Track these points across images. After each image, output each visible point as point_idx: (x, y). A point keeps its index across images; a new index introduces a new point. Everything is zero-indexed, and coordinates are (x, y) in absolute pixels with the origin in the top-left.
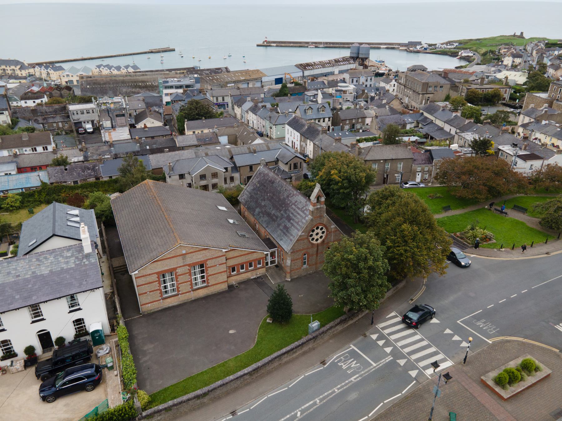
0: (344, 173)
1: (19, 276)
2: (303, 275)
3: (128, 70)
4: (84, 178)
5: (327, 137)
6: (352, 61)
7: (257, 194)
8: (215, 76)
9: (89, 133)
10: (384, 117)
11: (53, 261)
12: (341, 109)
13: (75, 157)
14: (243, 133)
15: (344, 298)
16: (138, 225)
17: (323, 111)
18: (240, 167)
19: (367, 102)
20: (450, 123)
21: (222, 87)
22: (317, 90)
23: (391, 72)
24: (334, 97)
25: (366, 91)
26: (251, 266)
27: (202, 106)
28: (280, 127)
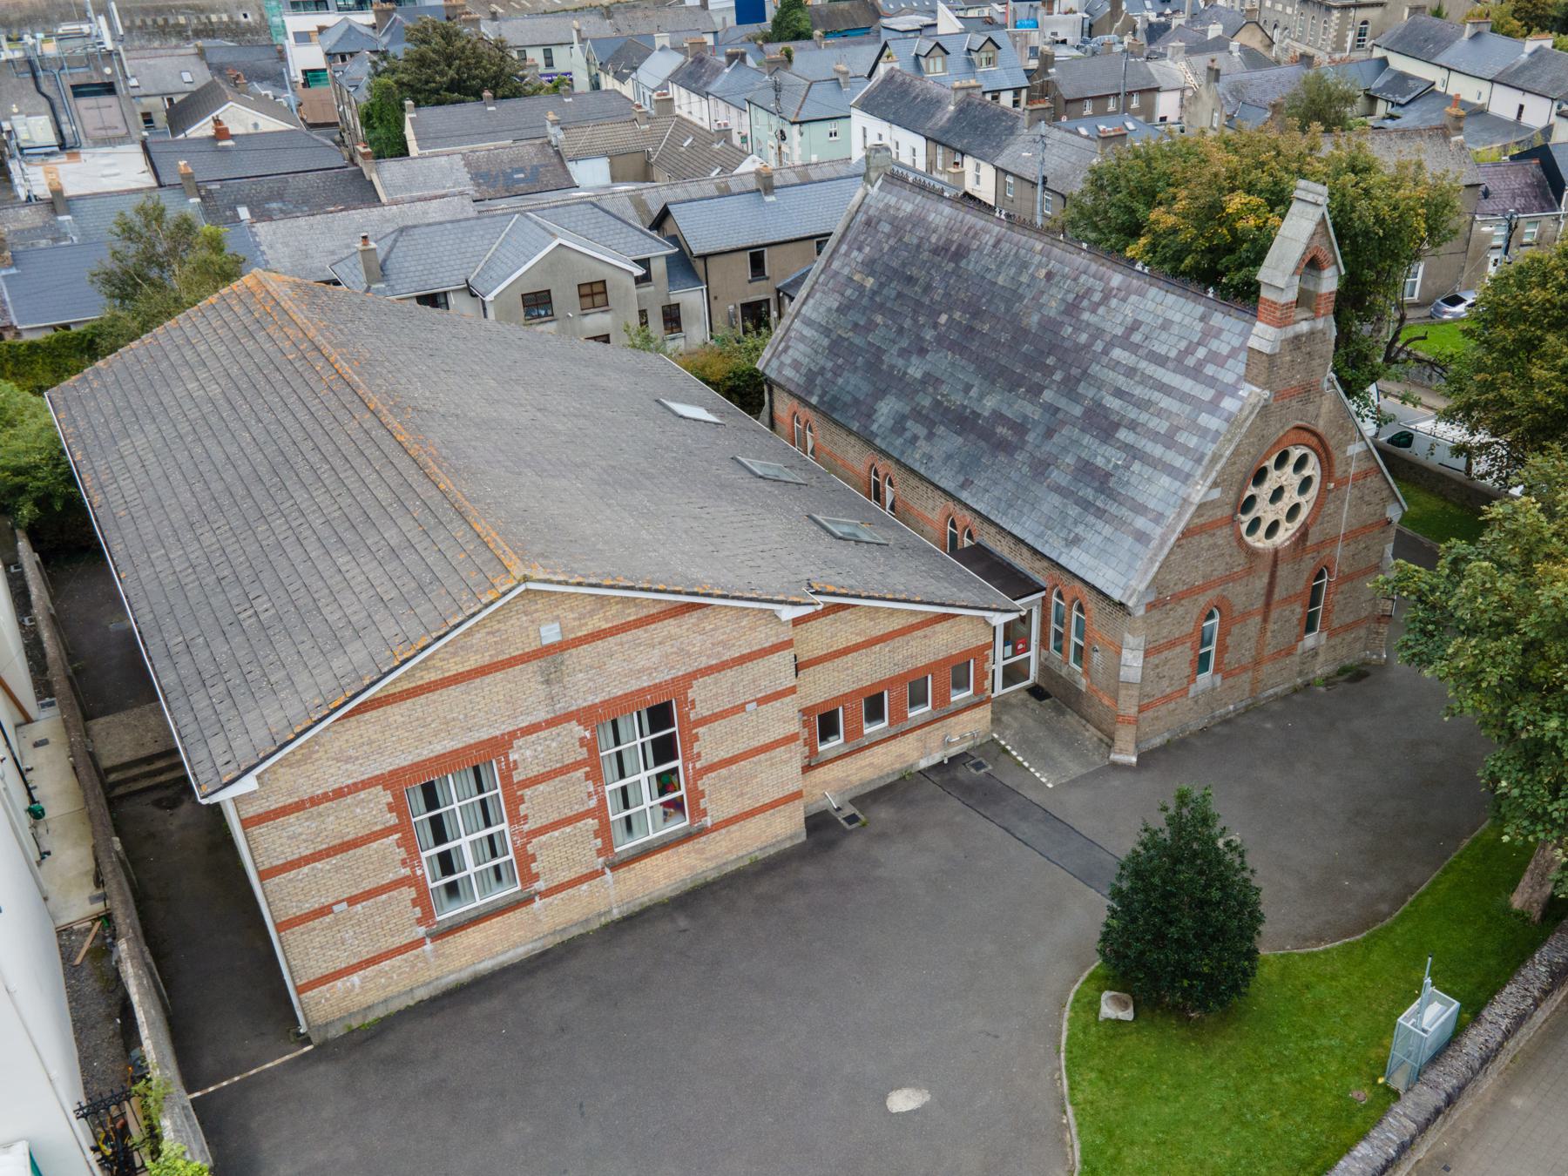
2: (1195, 725)
7: (871, 326)
16: (225, 501)
17: (989, 61)
18: (704, 257)
20: (1518, 83)
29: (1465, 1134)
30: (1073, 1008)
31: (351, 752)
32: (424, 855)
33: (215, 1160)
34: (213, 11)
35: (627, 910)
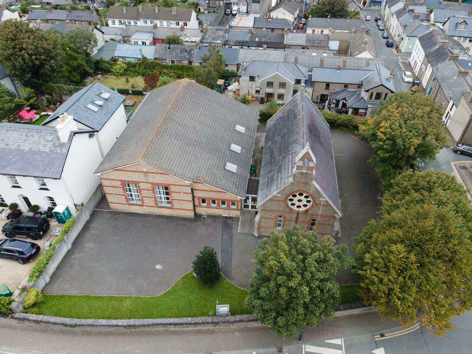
1: (8, 145)
11: (36, 140)
13: (195, 37)
18: (315, 82)
29: (222, 331)
35: (160, 214)
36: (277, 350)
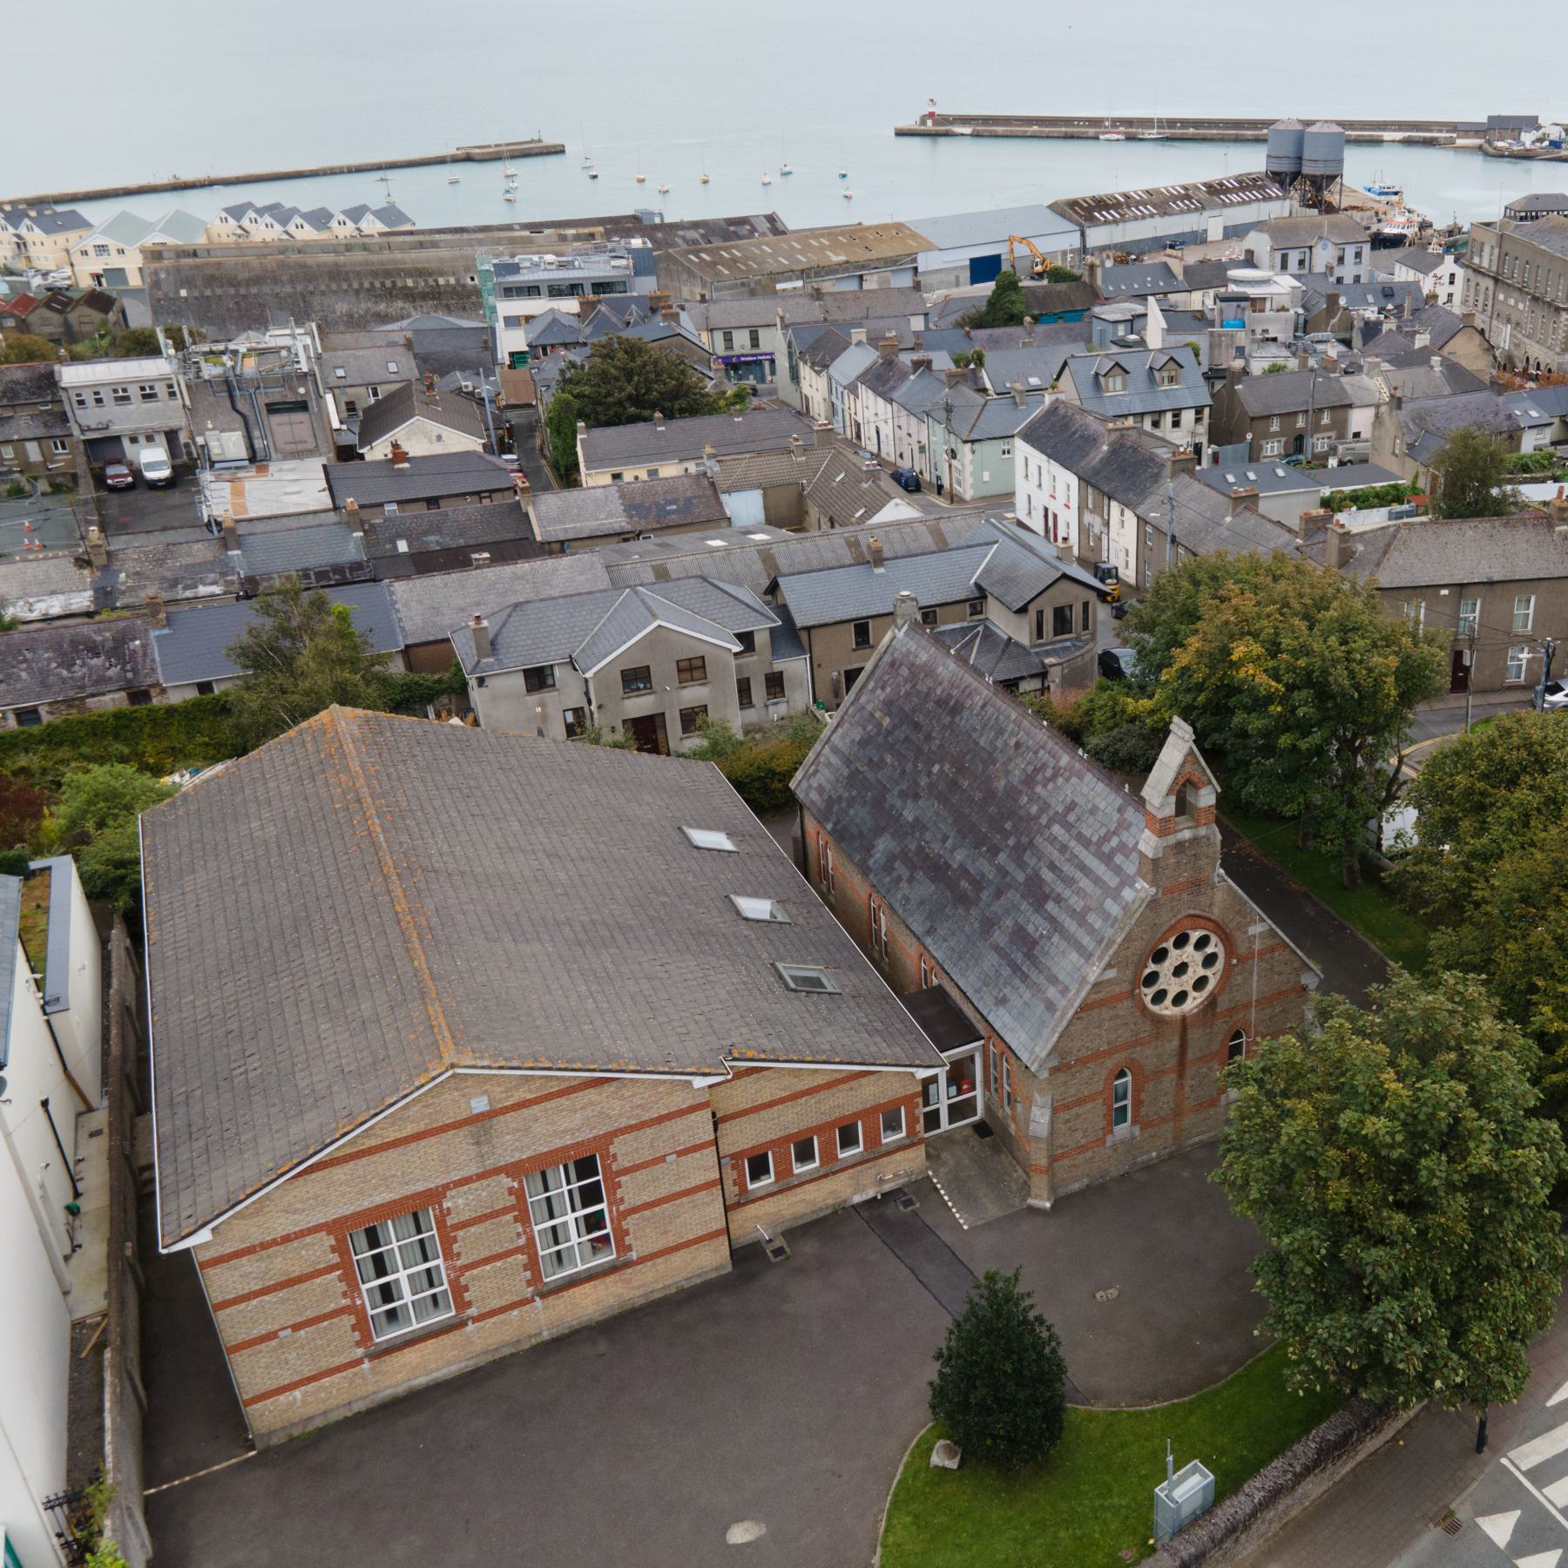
0: (1295, 653)
2: (1114, 1173)
3: (363, 225)
4: (71, 694)
5: (1197, 487)
6: (1275, 190)
8: (726, 249)
9: (153, 485)
10: (1431, 403)
12: (1245, 372)
13: (53, 593)
14: (828, 476)
15: (1342, 1350)
17: (1171, 380)
18: (808, 629)
19: (1347, 343)
21: (753, 293)
22: (1142, 298)
23: (1430, 231)
24: (1212, 324)
25: (1342, 301)
26: (848, 1139)
27: (655, 363)
28: (991, 449)
30: (912, 1455)
31: (300, 1206)
32: (364, 1287)
33: (155, 1552)
34: (441, 275)
35: (556, 1332)
36: (1439, 1529)
